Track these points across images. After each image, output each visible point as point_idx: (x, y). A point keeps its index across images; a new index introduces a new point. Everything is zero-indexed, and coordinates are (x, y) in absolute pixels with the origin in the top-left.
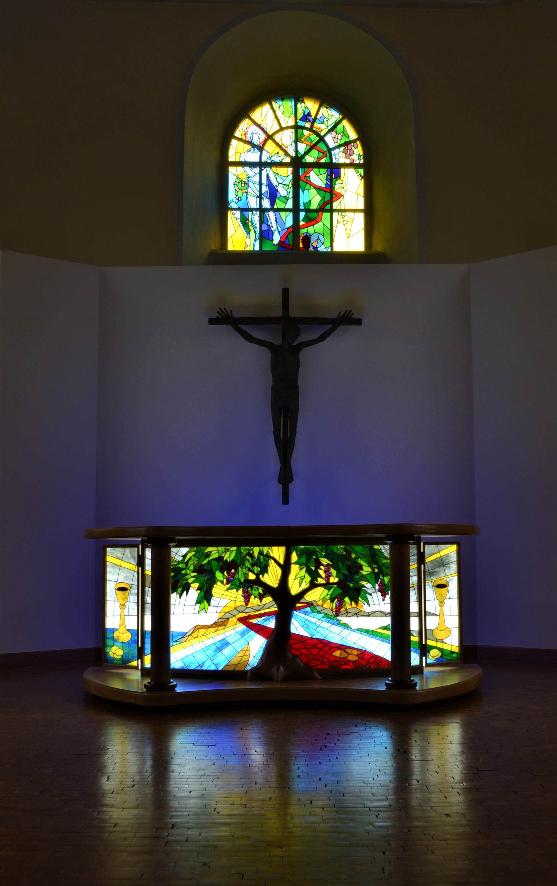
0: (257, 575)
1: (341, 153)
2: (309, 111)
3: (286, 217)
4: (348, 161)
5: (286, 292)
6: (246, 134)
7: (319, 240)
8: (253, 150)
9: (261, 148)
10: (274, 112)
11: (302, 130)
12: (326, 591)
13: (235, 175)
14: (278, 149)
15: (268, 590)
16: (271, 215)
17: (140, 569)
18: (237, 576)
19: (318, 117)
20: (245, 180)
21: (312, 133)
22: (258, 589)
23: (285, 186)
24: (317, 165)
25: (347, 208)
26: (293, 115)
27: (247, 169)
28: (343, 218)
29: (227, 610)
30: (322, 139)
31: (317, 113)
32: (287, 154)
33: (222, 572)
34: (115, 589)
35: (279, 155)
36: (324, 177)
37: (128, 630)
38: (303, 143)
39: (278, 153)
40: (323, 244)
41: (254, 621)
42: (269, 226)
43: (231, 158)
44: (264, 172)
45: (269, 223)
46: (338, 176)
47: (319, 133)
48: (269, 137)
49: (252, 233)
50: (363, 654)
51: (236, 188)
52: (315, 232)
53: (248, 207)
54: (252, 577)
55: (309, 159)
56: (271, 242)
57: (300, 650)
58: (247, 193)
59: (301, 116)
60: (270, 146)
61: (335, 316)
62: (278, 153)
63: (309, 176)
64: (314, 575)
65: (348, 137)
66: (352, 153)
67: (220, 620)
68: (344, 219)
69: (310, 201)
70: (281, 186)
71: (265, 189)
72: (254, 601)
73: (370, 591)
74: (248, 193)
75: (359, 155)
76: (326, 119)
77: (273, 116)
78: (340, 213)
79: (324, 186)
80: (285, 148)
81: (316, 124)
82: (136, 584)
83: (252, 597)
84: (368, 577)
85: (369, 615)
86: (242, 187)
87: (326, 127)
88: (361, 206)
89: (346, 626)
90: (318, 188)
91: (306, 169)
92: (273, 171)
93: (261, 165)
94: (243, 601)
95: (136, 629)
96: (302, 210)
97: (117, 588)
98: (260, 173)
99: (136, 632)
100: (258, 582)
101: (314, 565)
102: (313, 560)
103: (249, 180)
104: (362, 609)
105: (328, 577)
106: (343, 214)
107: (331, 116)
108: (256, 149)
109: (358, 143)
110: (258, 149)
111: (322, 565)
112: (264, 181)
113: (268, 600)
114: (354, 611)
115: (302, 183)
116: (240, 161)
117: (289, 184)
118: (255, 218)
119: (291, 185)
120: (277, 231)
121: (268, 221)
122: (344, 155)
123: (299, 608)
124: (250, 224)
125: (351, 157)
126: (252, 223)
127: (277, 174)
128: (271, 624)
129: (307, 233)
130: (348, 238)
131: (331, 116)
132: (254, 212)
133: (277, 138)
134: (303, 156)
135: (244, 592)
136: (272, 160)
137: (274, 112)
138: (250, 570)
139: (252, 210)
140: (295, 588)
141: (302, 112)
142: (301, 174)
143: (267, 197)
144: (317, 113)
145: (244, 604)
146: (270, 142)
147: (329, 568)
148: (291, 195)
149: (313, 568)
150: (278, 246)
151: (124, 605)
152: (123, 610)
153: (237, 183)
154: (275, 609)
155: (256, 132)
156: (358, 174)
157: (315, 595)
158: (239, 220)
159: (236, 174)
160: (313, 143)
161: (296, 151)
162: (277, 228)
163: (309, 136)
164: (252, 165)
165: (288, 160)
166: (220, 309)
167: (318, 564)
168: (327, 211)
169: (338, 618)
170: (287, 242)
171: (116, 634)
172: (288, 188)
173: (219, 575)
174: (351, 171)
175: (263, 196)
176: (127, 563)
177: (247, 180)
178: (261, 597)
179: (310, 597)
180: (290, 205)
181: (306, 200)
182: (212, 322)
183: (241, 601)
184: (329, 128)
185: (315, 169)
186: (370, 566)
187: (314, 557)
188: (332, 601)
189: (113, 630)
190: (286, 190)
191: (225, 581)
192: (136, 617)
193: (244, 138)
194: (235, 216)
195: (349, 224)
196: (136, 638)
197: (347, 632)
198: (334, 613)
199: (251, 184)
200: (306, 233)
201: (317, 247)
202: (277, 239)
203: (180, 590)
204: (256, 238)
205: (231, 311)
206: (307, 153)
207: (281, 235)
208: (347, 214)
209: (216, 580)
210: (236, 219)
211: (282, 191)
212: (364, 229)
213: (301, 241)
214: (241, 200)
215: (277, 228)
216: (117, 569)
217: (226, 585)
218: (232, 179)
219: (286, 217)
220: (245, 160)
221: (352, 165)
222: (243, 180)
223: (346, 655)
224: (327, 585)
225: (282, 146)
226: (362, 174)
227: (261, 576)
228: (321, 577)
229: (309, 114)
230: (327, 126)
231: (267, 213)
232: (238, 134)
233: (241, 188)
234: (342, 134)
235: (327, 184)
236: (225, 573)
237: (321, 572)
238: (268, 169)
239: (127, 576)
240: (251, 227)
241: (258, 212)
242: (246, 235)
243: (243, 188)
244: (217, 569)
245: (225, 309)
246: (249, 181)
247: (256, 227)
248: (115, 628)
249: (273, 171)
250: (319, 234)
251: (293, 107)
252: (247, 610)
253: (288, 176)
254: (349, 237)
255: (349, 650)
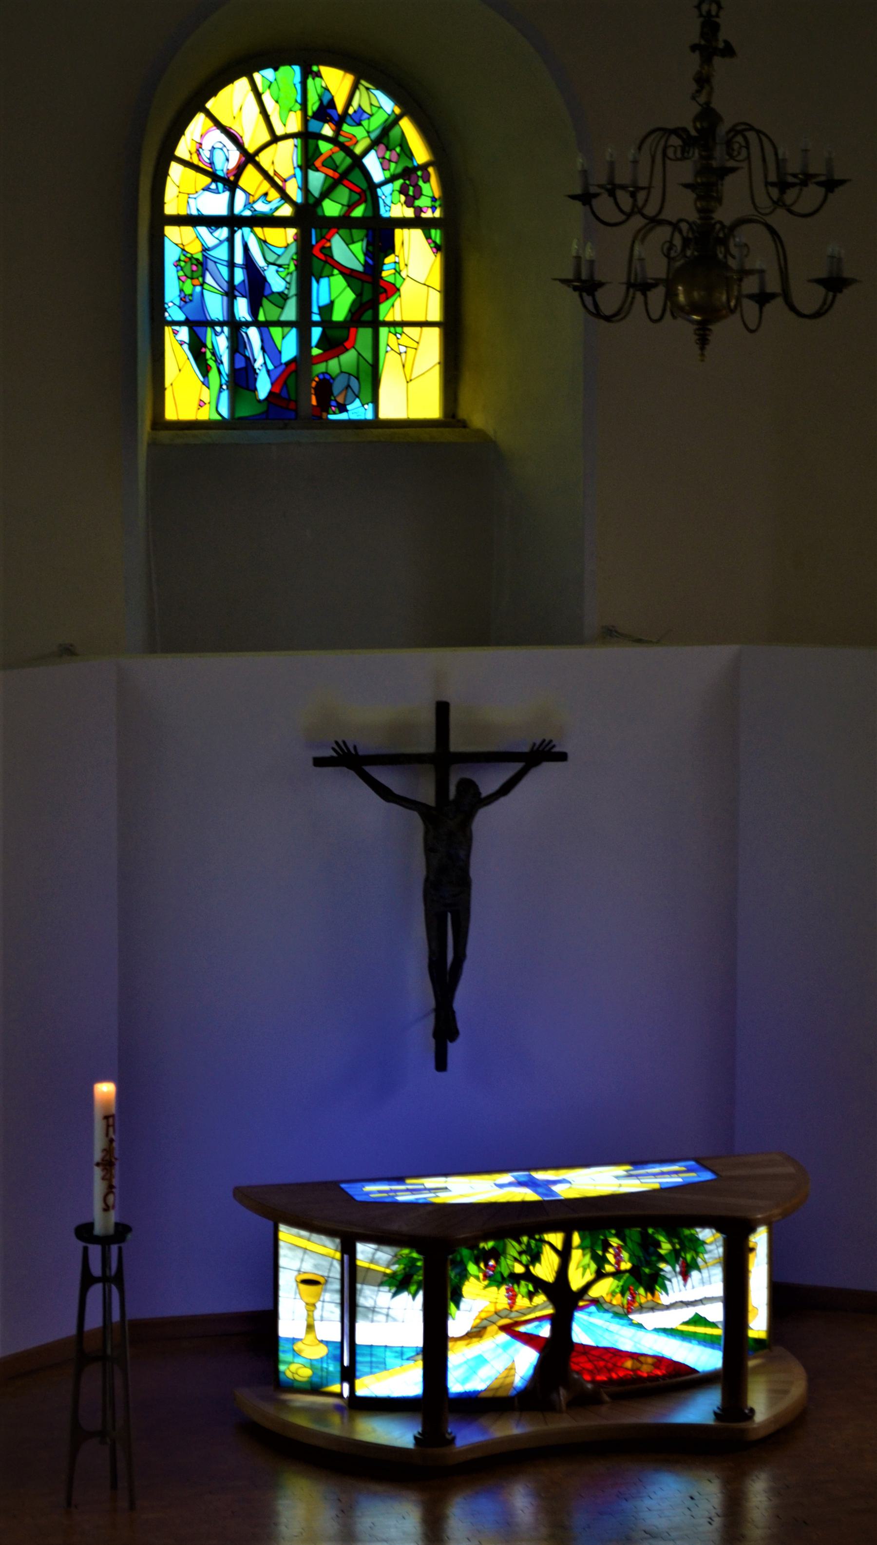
0: (527, 1267)
1: (396, 194)
2: (329, 97)
3: (283, 338)
4: (409, 213)
5: (442, 709)
6: (200, 150)
7: (350, 390)
8: (213, 186)
9: (231, 183)
10: (258, 96)
11: (315, 141)
12: (616, 1282)
13: (176, 245)
14: (266, 186)
15: (539, 1285)
16: (253, 334)
17: (346, 1256)
18: (498, 1269)
19: (351, 111)
20: (199, 256)
21: (337, 149)
22: (527, 1286)
23: (281, 269)
24: (344, 222)
25: (407, 318)
26: (298, 107)
27: (203, 230)
28: (398, 338)
29: (483, 1315)
30: (357, 162)
31: (349, 103)
32: (285, 197)
33: (477, 1263)
34: (296, 1281)
35: (269, 198)
36: (358, 248)
37: (321, 1341)
38: (317, 170)
39: (266, 194)
40: (357, 396)
41: (522, 1329)
42: (247, 359)
43: (170, 209)
44: (238, 236)
45: (248, 353)
46: (389, 248)
47: (352, 147)
48: (249, 158)
49: (213, 375)
50: (660, 1361)
51: (181, 273)
52: (342, 372)
53: (204, 319)
54: (519, 1269)
55: (331, 209)
56: (251, 393)
57: (581, 1365)
58: (202, 285)
59: (315, 108)
60: (250, 179)
61: (526, 749)
62: (266, 194)
63: (330, 248)
64: (600, 1261)
65: (410, 156)
66: (418, 194)
67: (475, 1330)
68: (400, 342)
69: (332, 303)
70: (273, 268)
71: (239, 276)
72: (522, 1302)
73: (668, 1276)
74: (206, 286)
75: (434, 199)
76: (365, 116)
77: (256, 109)
78: (392, 329)
79: (360, 268)
80: (280, 183)
81: (346, 128)
82: (338, 1276)
83: (519, 1296)
84: (667, 1258)
85: (668, 1307)
86: (193, 271)
87: (366, 134)
88: (435, 314)
89: (640, 1326)
90: (348, 274)
91: (324, 231)
92: (255, 235)
93: (233, 222)
94: (506, 1302)
95: (339, 1339)
96: (316, 324)
97: (298, 1280)
98: (231, 240)
99: (339, 1345)
100: (528, 1276)
101: (601, 1248)
102: (600, 1242)
103: (207, 255)
104: (660, 1302)
105: (618, 1263)
106: (399, 329)
107: (375, 109)
108: (220, 185)
109: (431, 170)
110: (224, 185)
111: (611, 1246)
112: (239, 258)
113: (540, 1299)
114: (650, 1304)
115: (317, 264)
116: (189, 213)
117: (288, 265)
118: (220, 342)
119: (292, 268)
120: (264, 371)
121: (245, 347)
122: (403, 198)
123: (582, 1308)
124: (209, 355)
125: (417, 203)
126: (214, 354)
127: (265, 242)
128: (545, 1331)
129: (327, 373)
130: (408, 382)
131: (376, 109)
132: (218, 329)
133: (263, 159)
134: (319, 202)
135: (508, 1290)
136: (255, 210)
137: (258, 96)
138: (516, 1260)
139: (213, 324)
140: (576, 1280)
141: (316, 98)
142: (314, 242)
143: (244, 294)
144: (349, 103)
145: (507, 1307)
146: (250, 169)
147: (620, 1251)
148: (293, 291)
149: (600, 1253)
150: (265, 403)
151: (314, 1305)
152: (311, 1313)
153: (182, 264)
154: (550, 1311)
155: (220, 146)
156: (430, 241)
157: (603, 1289)
158: (186, 347)
159: (178, 241)
160: (340, 170)
161: (305, 188)
162: (265, 363)
163: (330, 156)
164: (212, 222)
165: (286, 211)
166: (337, 743)
167: (606, 1246)
168: (365, 324)
169: (631, 1316)
170: (284, 394)
171: (298, 1346)
172: (288, 274)
173: (472, 1268)
174: (417, 234)
175: (237, 293)
176: (319, 1245)
177: (204, 255)
178: (531, 1295)
179: (594, 1292)
180: (290, 312)
181: (324, 301)
182: (319, 762)
183: (503, 1302)
184: (374, 136)
185: (341, 231)
186: (671, 1242)
187: (602, 1237)
188: (623, 1294)
189: (294, 1341)
190: (284, 279)
191: (481, 1276)
192: (339, 1325)
193: (195, 160)
194: (179, 337)
195: (411, 352)
196: (338, 1352)
197: (641, 1333)
198: (626, 1310)
199: (210, 265)
200: (323, 373)
201: (346, 403)
202: (264, 387)
203: (413, 1288)
204: (221, 386)
205: (355, 747)
206: (326, 193)
207: (274, 378)
208: (407, 330)
209: (468, 1276)
210: (181, 345)
211: (276, 282)
212: (439, 363)
213: (313, 391)
214: (191, 301)
215: (265, 363)
216: (300, 1253)
217: (482, 1282)
218: (171, 254)
219: (283, 338)
220: (198, 210)
221: (417, 223)
222: (195, 256)
223: (638, 1365)
224: (617, 1274)
225: (276, 179)
226: (438, 241)
227: (531, 1268)
228: (609, 1263)
229: (332, 104)
230: (368, 132)
231: (244, 329)
232: (183, 149)
233: (189, 274)
234: (398, 149)
235: (366, 265)
236: (482, 1265)
237: (610, 1257)
238: (246, 230)
239: (319, 1265)
240: (211, 363)
241: (226, 329)
242: (202, 379)
243: (195, 275)
244: (470, 1259)
245: (344, 742)
246: (207, 257)
247: (222, 363)
248: (295, 1337)
249: (255, 235)
250: (350, 374)
251: (299, 86)
252: (513, 1315)
253: (286, 247)
254: (411, 380)
255: (642, 1359)
